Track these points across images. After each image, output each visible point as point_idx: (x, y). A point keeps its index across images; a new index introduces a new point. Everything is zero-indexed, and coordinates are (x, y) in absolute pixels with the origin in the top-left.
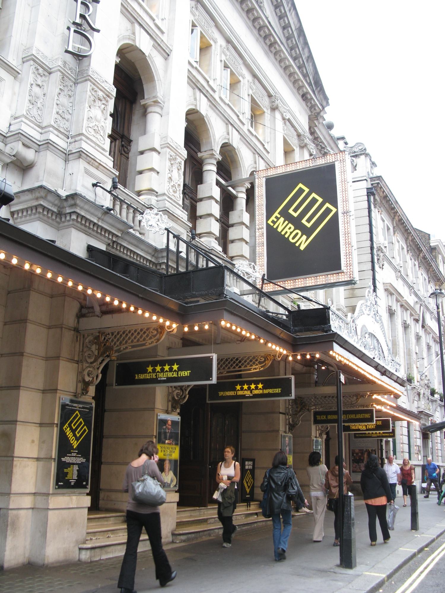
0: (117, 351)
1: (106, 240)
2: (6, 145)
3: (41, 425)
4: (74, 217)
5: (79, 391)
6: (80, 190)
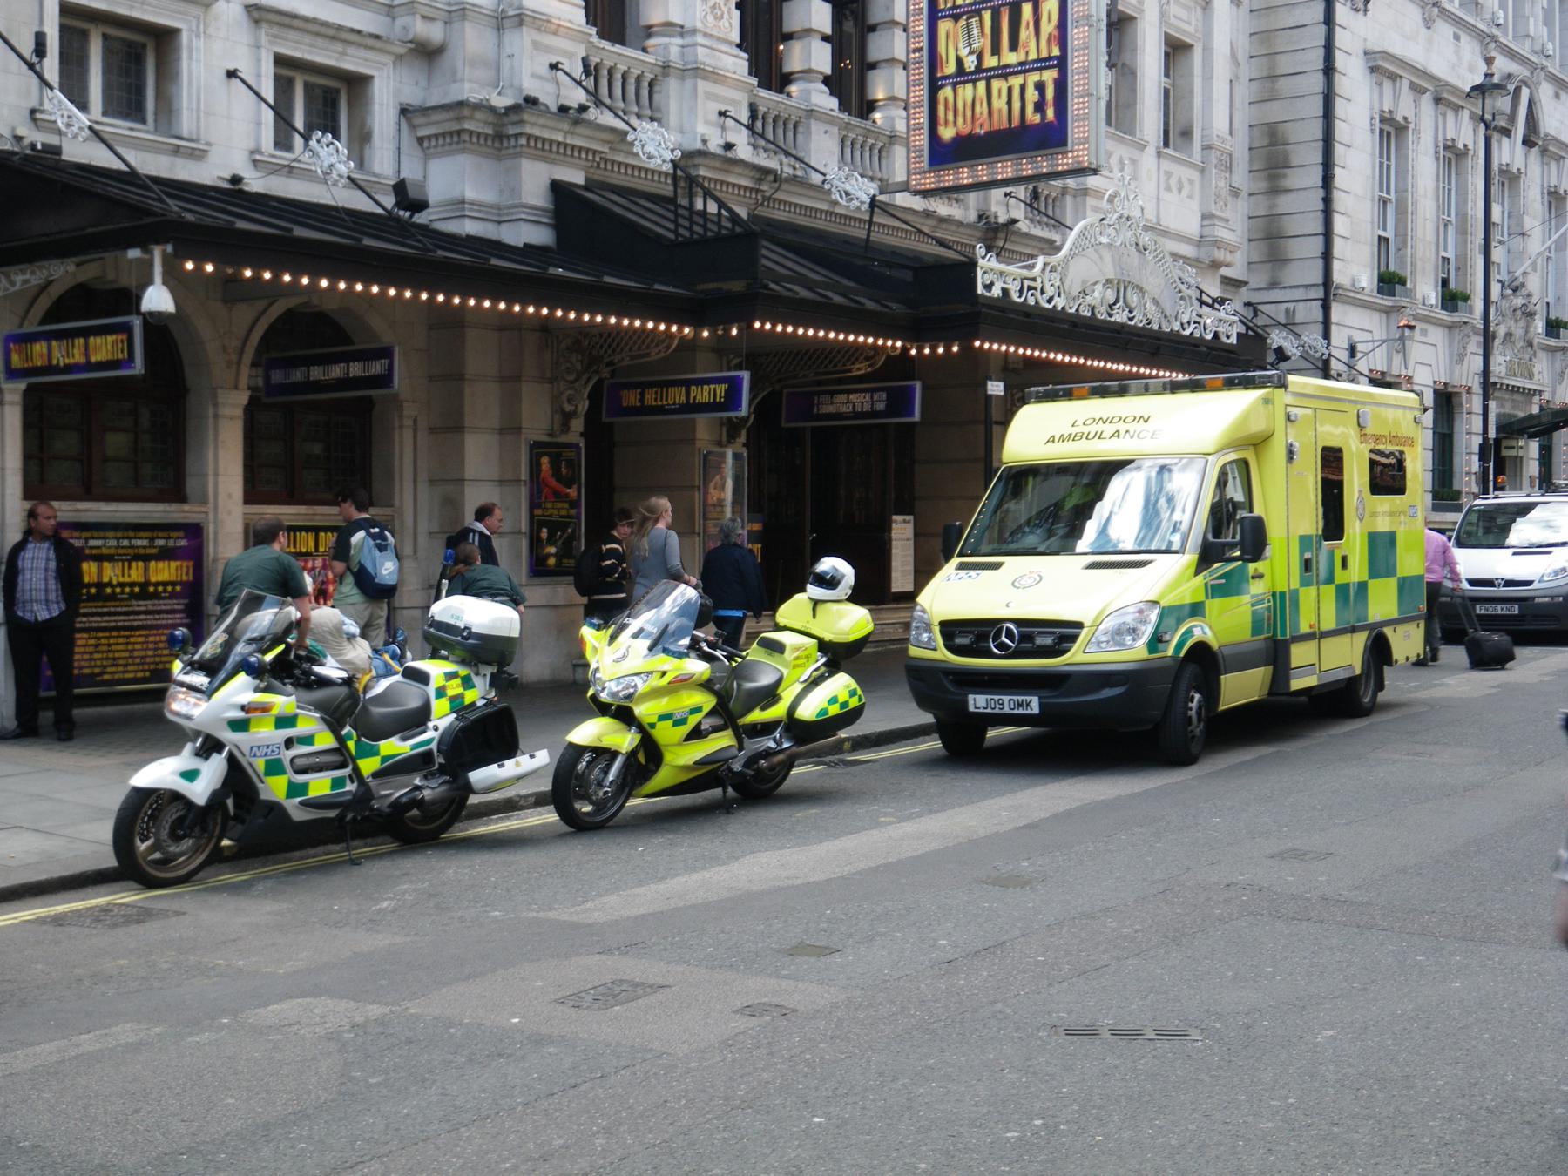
0: (609, 364)
1: (583, 163)
2: (394, 19)
3: (501, 482)
4: (523, 141)
5: (557, 426)
6: (531, 87)
